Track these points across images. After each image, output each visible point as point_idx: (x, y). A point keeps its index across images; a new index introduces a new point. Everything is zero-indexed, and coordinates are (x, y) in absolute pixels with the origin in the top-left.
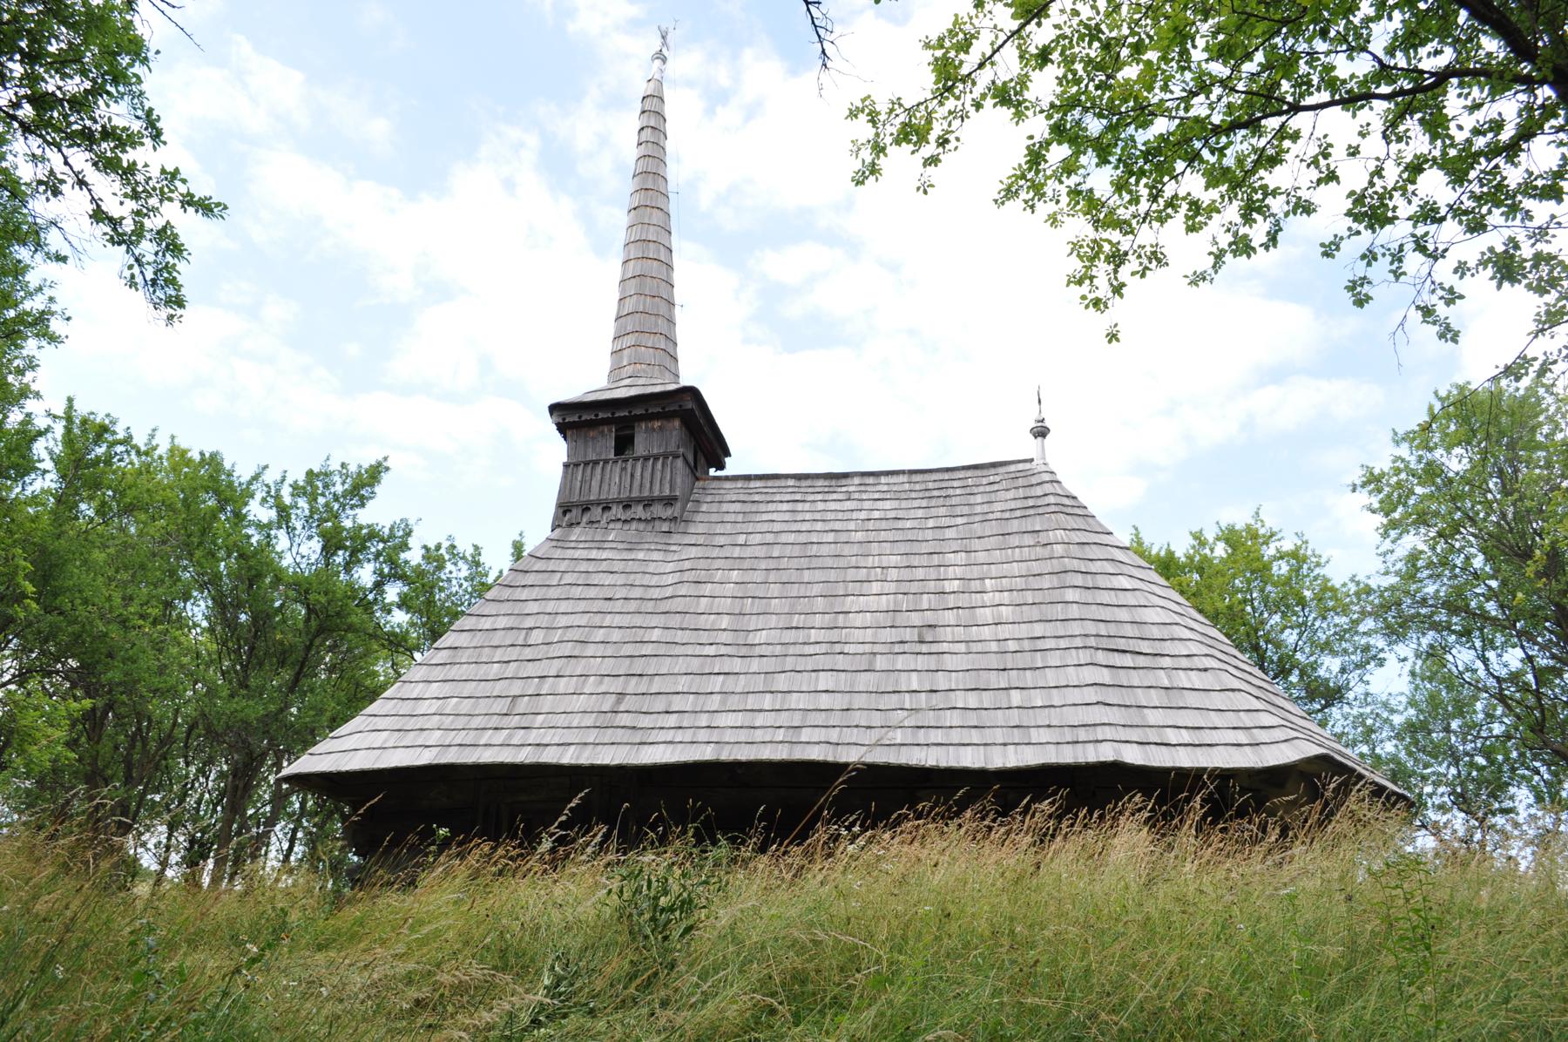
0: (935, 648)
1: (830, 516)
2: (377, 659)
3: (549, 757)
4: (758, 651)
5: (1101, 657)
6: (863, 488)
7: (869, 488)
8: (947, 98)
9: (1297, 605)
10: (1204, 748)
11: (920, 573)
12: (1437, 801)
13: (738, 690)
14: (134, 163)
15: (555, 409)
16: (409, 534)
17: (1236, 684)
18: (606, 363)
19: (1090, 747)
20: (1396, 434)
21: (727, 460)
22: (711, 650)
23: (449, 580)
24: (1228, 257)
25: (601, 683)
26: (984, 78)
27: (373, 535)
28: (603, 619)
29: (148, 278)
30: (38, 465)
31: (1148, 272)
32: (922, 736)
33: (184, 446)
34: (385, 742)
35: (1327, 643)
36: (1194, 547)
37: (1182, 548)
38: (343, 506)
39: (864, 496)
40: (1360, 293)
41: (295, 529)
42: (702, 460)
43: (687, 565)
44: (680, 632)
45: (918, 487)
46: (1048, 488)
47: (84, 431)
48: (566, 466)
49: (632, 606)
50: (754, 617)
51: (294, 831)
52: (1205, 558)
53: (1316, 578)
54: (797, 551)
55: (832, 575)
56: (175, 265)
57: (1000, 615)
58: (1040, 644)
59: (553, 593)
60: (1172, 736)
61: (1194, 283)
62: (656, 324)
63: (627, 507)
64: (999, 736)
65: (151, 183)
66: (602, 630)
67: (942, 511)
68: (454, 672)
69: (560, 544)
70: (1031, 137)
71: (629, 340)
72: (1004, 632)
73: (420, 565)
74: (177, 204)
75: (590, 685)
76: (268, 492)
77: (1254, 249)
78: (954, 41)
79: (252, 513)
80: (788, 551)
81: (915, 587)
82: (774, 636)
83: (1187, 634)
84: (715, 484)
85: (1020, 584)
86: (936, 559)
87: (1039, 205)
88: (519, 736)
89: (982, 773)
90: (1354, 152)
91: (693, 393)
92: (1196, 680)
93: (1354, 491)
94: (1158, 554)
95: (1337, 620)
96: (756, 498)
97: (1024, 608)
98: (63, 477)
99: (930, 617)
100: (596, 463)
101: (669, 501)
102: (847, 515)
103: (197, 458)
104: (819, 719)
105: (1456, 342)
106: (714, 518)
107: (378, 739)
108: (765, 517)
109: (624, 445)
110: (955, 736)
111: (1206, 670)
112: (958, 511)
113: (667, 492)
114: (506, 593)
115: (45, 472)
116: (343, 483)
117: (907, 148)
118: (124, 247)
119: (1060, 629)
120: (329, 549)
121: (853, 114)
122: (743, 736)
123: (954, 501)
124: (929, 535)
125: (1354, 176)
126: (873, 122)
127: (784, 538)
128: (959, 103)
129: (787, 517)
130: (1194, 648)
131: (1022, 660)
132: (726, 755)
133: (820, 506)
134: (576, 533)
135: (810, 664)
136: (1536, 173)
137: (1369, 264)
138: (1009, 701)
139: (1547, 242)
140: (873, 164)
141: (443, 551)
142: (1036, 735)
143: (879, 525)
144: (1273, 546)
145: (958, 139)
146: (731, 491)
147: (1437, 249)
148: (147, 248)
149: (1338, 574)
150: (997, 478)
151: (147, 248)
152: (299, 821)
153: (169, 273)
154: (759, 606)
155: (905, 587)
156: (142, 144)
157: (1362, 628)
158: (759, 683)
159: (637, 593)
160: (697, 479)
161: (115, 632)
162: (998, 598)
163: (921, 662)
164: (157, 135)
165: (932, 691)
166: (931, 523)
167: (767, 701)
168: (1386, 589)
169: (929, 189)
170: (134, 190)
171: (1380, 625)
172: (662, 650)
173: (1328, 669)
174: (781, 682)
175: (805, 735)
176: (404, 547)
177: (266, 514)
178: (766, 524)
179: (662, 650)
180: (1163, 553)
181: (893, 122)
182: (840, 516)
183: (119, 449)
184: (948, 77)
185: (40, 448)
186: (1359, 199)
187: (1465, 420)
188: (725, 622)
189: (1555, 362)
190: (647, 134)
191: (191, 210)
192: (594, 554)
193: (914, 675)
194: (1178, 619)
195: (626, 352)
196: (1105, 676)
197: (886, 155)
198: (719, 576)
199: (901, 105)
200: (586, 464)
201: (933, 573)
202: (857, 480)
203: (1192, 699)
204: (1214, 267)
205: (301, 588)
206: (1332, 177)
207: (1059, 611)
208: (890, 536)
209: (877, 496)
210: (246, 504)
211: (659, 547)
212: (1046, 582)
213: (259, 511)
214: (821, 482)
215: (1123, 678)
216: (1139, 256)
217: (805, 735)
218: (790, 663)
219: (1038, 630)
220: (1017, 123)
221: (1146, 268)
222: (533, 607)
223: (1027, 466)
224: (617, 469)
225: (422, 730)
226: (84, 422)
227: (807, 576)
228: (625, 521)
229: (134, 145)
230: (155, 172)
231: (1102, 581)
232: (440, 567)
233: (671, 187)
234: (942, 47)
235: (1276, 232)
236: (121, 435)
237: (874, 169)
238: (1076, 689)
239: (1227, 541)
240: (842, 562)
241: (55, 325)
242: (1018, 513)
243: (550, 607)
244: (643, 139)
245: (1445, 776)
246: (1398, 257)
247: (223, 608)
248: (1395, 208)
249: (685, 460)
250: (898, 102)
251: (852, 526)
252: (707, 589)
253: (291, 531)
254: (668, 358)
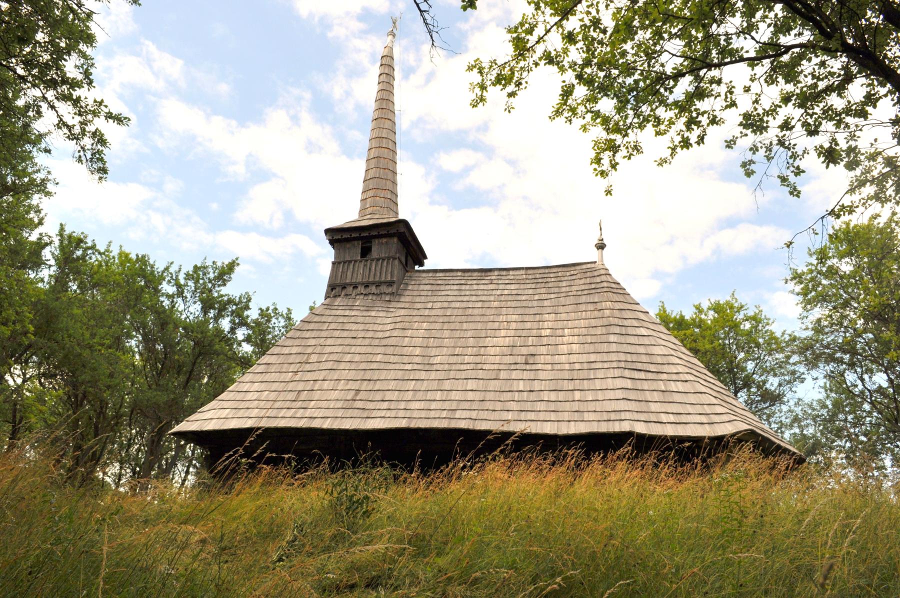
0: (534, 367)
1: (480, 293)
2: (235, 372)
4: (435, 367)
5: (627, 373)
6: (499, 277)
7: (503, 278)
8: (521, 60)
9: (755, 347)
10: (682, 425)
11: (528, 325)
12: (839, 461)
13: (423, 389)
14: (80, 97)
15: (328, 231)
16: (249, 300)
17: (703, 389)
18: (357, 206)
19: (617, 423)
20: (810, 250)
21: (425, 261)
22: (409, 367)
23: (274, 328)
24: (679, 149)
25: (347, 384)
26: (540, 50)
27: (230, 301)
28: (351, 349)
29: (88, 158)
30: (47, 262)
31: (632, 157)
32: (523, 416)
33: (127, 251)
34: (228, 414)
35: (772, 369)
36: (696, 313)
37: (689, 314)
38: (214, 285)
39: (500, 282)
40: (748, 169)
41: (186, 298)
42: (410, 261)
43: (399, 319)
44: (392, 357)
45: (530, 277)
46: (603, 278)
47: (70, 242)
48: (333, 263)
49: (367, 342)
50: (434, 349)
51: (188, 467)
52: (701, 320)
53: (766, 332)
54: (460, 312)
55: (479, 326)
56: (102, 150)
57: (572, 349)
58: (593, 366)
59: (324, 334)
60: (664, 418)
61: (660, 164)
62: (386, 184)
63: (367, 286)
64: (566, 416)
65: (88, 107)
66: (349, 355)
67: (543, 291)
68: (267, 377)
69: (329, 307)
70: (564, 82)
71: (370, 193)
72: (573, 358)
73: (258, 319)
74: (103, 118)
75: (341, 385)
76: (172, 277)
77: (691, 145)
78: (524, 28)
79: (164, 289)
80: (455, 312)
81: (525, 333)
82: (444, 359)
83: (678, 361)
84: (417, 274)
85: (584, 331)
86: (538, 318)
87: (574, 120)
88: (300, 413)
89: (555, 437)
90: (747, 90)
91: (405, 223)
92: (680, 387)
93: (786, 283)
94: (675, 317)
95: (777, 356)
96: (439, 282)
97: (586, 345)
98: (59, 268)
99: (532, 350)
100: (350, 262)
101: (390, 284)
102: (490, 293)
103: (134, 257)
104: (466, 405)
105: (799, 197)
106: (415, 293)
107: (224, 413)
108: (444, 293)
109: (365, 252)
110: (542, 416)
111: (686, 381)
112: (552, 290)
113: (389, 279)
114: (298, 334)
115: (50, 266)
116: (214, 272)
117: (499, 87)
118: (75, 141)
119: (605, 357)
120: (205, 310)
121: (470, 68)
122: (423, 414)
123: (550, 285)
124: (535, 304)
125: (745, 104)
126: (481, 73)
127: (453, 305)
128: (526, 63)
129: (456, 293)
130: (680, 369)
131: (583, 375)
132: (414, 425)
133: (475, 287)
134: (338, 301)
135: (464, 375)
136: (852, 102)
137: (754, 153)
138: (574, 397)
139: (855, 140)
140: (482, 96)
141: (270, 311)
142: (587, 416)
143: (507, 298)
144: (742, 313)
145: (526, 82)
146: (426, 279)
147: (790, 144)
148: (87, 141)
149: (777, 329)
150: (575, 272)
151: (87, 141)
152: (191, 461)
153: (100, 155)
154: (437, 342)
155: (519, 333)
156: (83, 87)
157: (791, 361)
158: (434, 385)
159: (370, 334)
160: (407, 271)
161: (86, 353)
162: (571, 339)
163: (526, 375)
164: (90, 83)
165: (531, 391)
166: (536, 297)
167: (438, 395)
168: (805, 339)
169: (511, 110)
170: (79, 111)
171: (803, 359)
172: (382, 366)
173: (772, 385)
174: (447, 385)
175: (458, 414)
176: (247, 308)
177: (171, 289)
178: (444, 297)
179: (382, 366)
180: (678, 317)
181: (492, 73)
182: (486, 293)
183: (90, 252)
184: (521, 48)
185: (46, 253)
186: (747, 116)
187: (850, 242)
188: (418, 351)
189: (857, 207)
190: (384, 77)
191: (111, 121)
192: (347, 313)
193: (521, 382)
194: (672, 352)
195: (369, 200)
196: (629, 384)
197: (487, 91)
198: (416, 325)
199: (496, 64)
200: (345, 262)
201: (535, 325)
202: (496, 273)
203: (677, 398)
204: (671, 155)
205: (188, 328)
206: (733, 104)
207: (605, 347)
208: (513, 304)
209: (507, 282)
210: (161, 284)
211: (384, 309)
212: (599, 331)
213: (168, 288)
214: (476, 274)
215: (639, 384)
216: (627, 148)
217: (458, 414)
218: (452, 374)
219: (593, 357)
220: (562, 74)
221: (631, 154)
222: (312, 342)
223: (593, 265)
224: (362, 265)
225: (248, 408)
226: (70, 237)
227: (465, 326)
228: (365, 295)
229: (80, 87)
230: (90, 102)
231: (631, 331)
232: (269, 321)
233: (397, 107)
234: (516, 32)
235: (704, 135)
236: (90, 244)
237: (482, 99)
238: (612, 391)
239: (714, 310)
240: (485, 319)
241: (50, 187)
242: (586, 292)
243: (322, 341)
244: (381, 80)
245: (844, 447)
246: (769, 149)
247: (148, 341)
248: (767, 122)
250: (495, 62)
251: (492, 298)
252: (409, 333)
253: (184, 299)
254: (392, 203)
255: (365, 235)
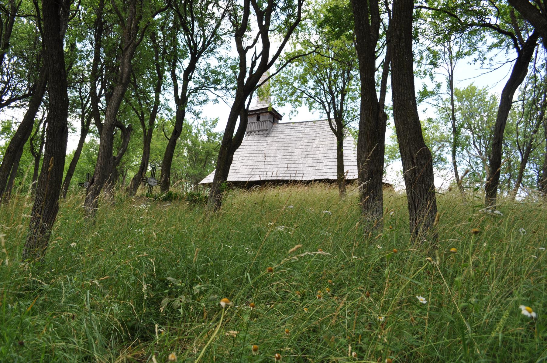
3: (240, 180)
27: (217, 134)
88: (236, 176)
101: (266, 130)
159: (259, 149)
192: (252, 142)
217: (317, 174)
218: (282, 162)
219: (326, 155)
249: (270, 121)
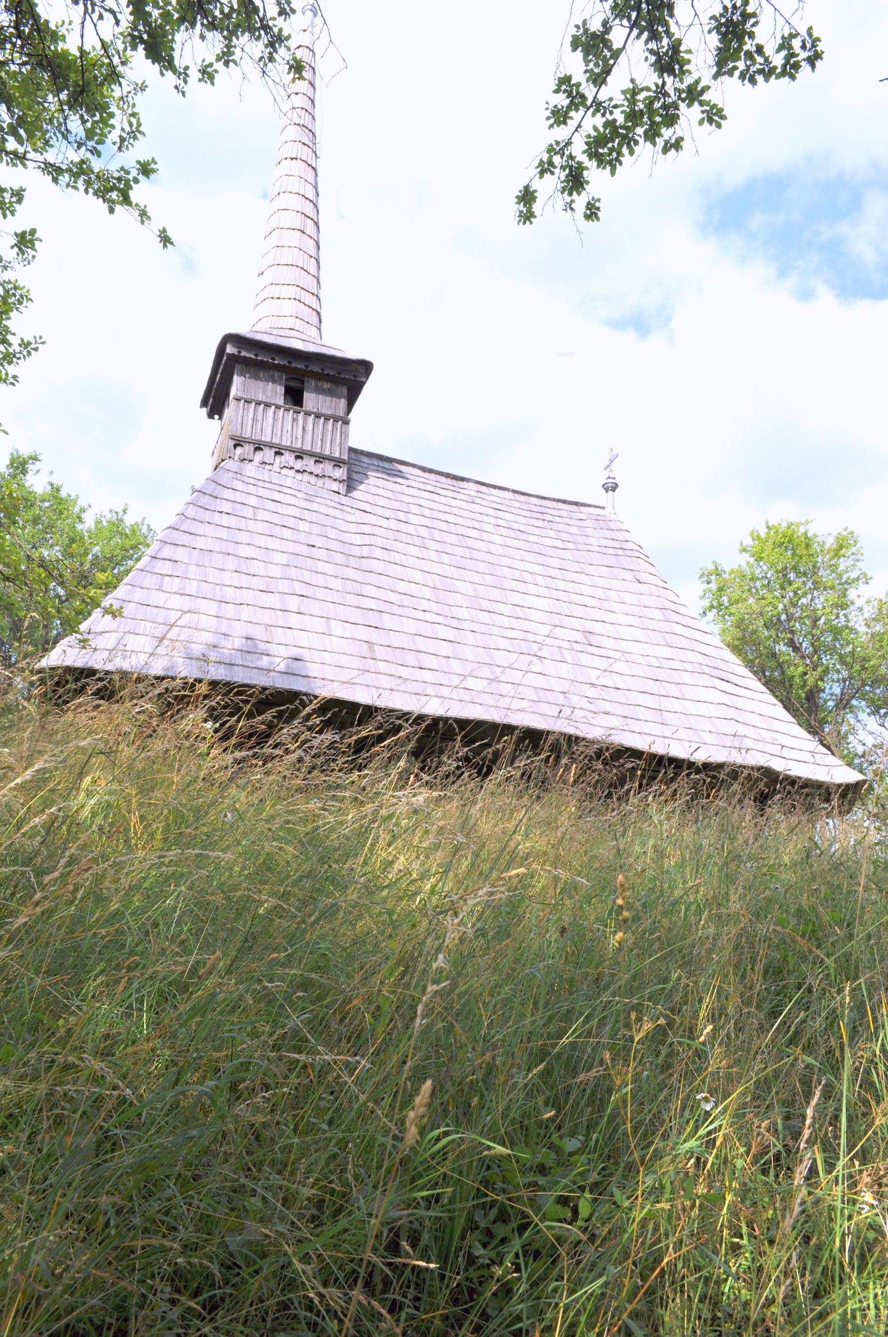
31: (573, 206)
109: (294, 397)
255: (299, 366)
